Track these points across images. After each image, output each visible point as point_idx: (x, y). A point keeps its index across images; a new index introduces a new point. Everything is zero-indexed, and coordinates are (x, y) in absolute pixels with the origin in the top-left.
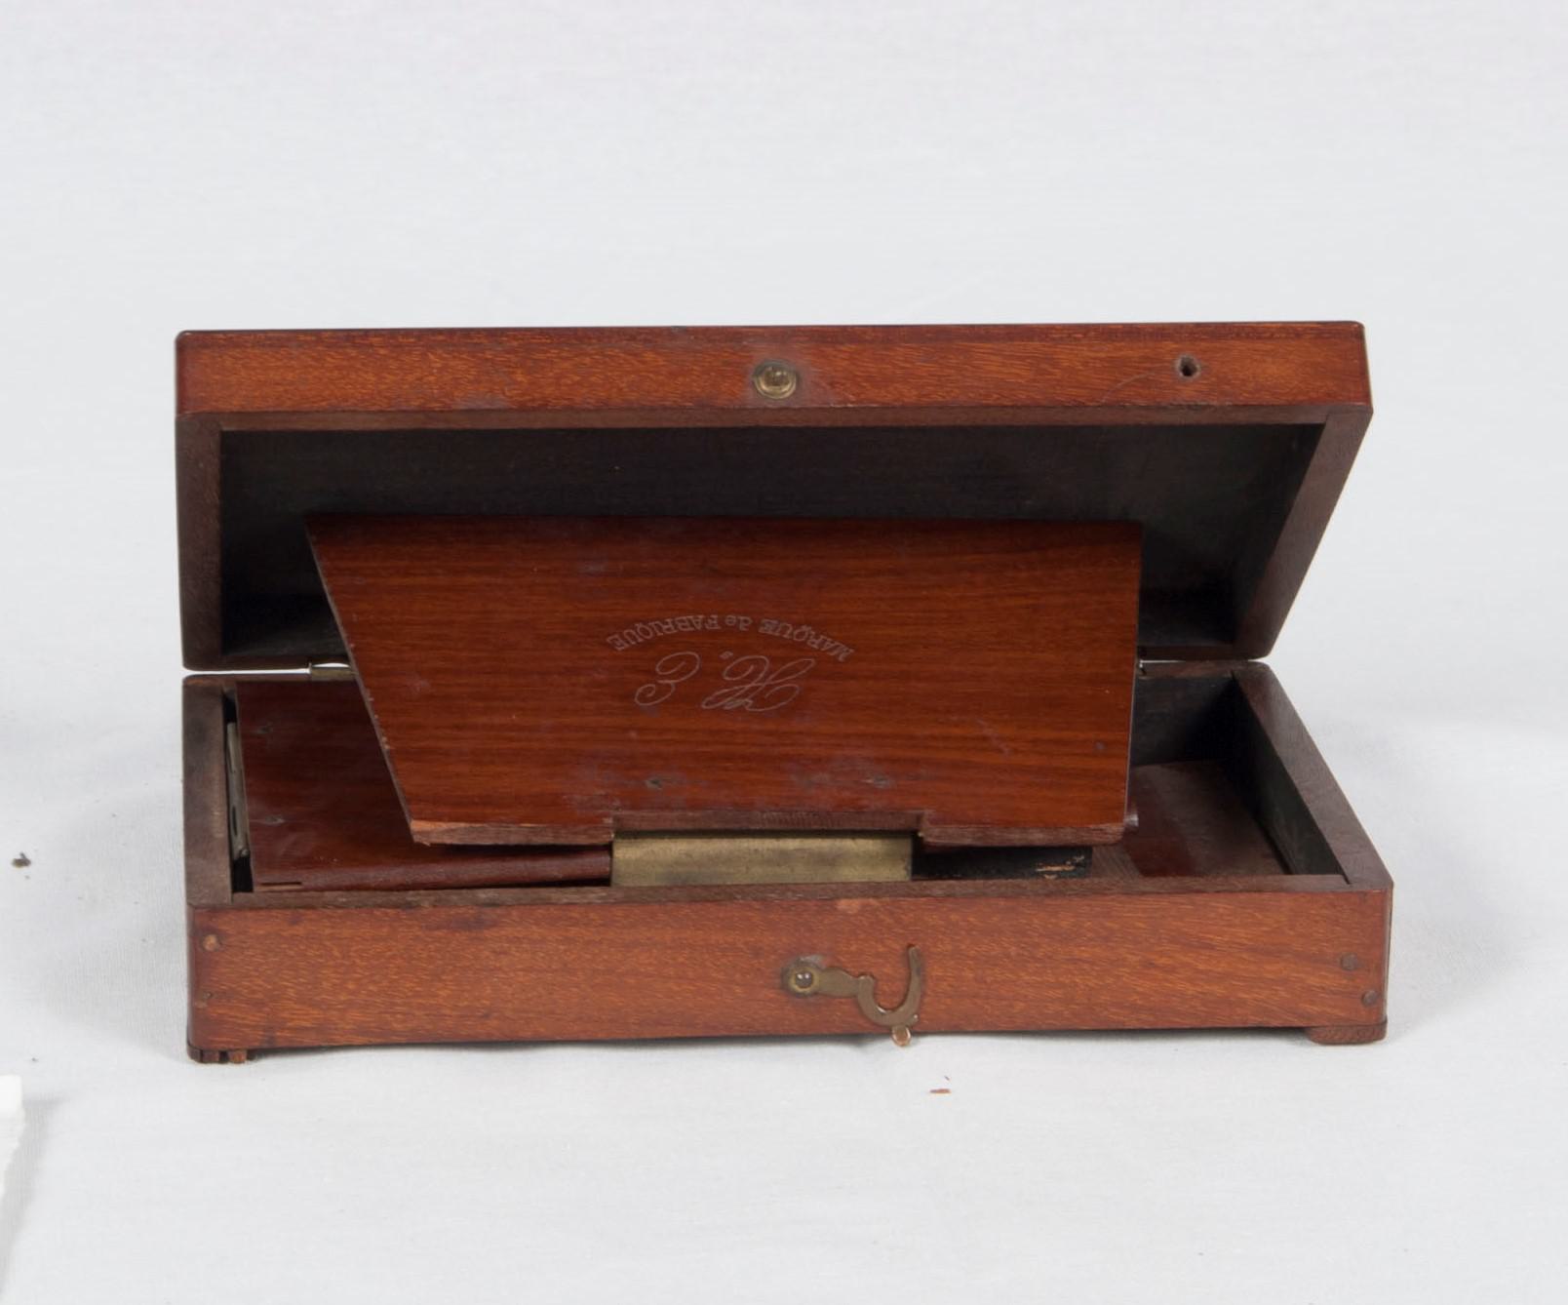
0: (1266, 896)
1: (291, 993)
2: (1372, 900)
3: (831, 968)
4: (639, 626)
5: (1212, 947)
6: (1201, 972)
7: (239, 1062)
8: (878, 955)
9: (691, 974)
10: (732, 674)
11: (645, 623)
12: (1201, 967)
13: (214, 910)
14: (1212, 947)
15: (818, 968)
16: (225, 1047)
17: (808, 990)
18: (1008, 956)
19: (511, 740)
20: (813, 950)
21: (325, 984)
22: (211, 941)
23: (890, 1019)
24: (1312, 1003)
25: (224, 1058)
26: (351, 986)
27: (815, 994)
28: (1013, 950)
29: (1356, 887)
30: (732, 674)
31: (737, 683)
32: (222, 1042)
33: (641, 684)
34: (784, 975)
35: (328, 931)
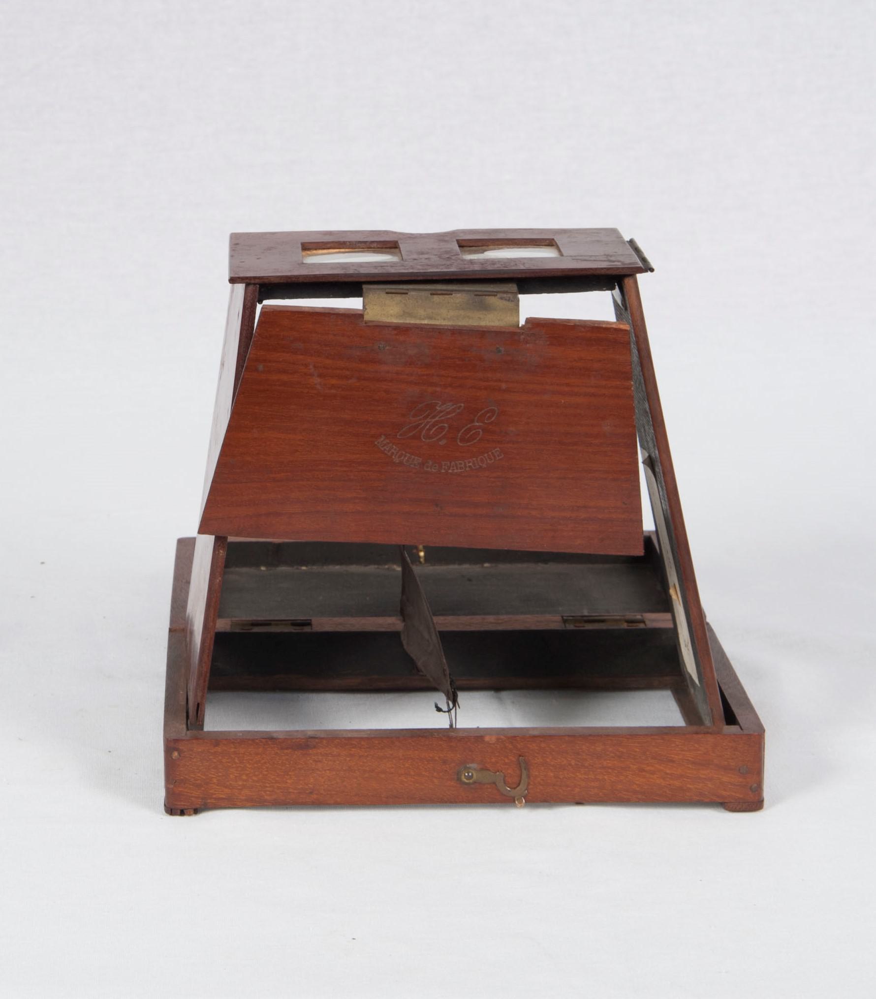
0: (700, 736)
1: (215, 781)
2: (755, 741)
3: (482, 769)
4: (484, 466)
5: (673, 761)
6: (667, 774)
7: (190, 815)
8: (506, 764)
9: (412, 773)
10: (442, 428)
11: (481, 467)
12: (668, 771)
13: (176, 741)
14: (673, 761)
15: (475, 769)
16: (182, 807)
17: (471, 781)
18: (570, 765)
19: (568, 385)
20: (473, 761)
21: (231, 776)
22: (176, 754)
23: (513, 793)
24: (725, 790)
25: (182, 813)
26: (244, 777)
27: (475, 783)
28: (573, 762)
29: (746, 732)
30: (442, 428)
31: (442, 422)
32: (181, 805)
33: (491, 423)
34: (458, 774)
35: (233, 750)
